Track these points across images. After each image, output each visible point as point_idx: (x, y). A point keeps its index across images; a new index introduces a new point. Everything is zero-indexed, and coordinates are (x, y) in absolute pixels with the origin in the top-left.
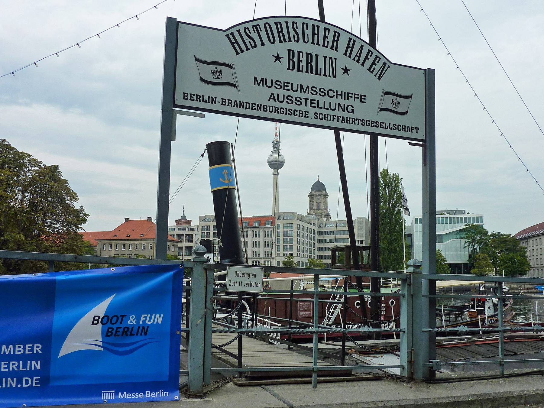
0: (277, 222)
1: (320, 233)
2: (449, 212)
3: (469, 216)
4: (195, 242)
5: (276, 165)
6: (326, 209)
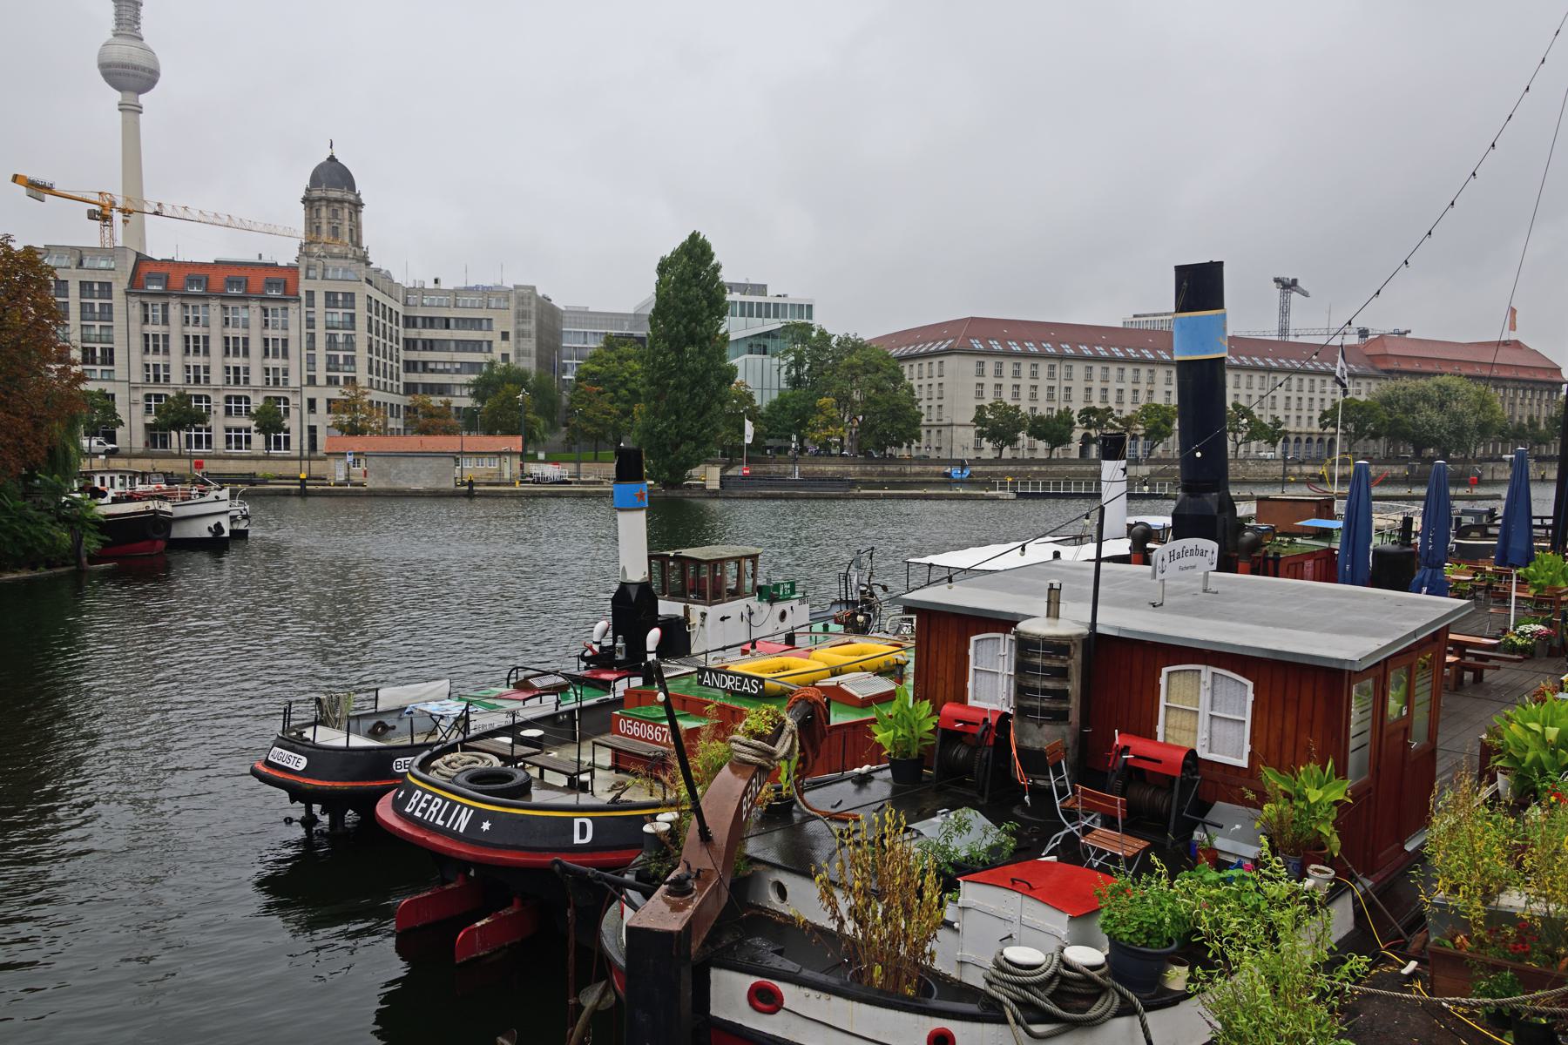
1: (410, 322)
5: (131, 78)
6: (358, 244)
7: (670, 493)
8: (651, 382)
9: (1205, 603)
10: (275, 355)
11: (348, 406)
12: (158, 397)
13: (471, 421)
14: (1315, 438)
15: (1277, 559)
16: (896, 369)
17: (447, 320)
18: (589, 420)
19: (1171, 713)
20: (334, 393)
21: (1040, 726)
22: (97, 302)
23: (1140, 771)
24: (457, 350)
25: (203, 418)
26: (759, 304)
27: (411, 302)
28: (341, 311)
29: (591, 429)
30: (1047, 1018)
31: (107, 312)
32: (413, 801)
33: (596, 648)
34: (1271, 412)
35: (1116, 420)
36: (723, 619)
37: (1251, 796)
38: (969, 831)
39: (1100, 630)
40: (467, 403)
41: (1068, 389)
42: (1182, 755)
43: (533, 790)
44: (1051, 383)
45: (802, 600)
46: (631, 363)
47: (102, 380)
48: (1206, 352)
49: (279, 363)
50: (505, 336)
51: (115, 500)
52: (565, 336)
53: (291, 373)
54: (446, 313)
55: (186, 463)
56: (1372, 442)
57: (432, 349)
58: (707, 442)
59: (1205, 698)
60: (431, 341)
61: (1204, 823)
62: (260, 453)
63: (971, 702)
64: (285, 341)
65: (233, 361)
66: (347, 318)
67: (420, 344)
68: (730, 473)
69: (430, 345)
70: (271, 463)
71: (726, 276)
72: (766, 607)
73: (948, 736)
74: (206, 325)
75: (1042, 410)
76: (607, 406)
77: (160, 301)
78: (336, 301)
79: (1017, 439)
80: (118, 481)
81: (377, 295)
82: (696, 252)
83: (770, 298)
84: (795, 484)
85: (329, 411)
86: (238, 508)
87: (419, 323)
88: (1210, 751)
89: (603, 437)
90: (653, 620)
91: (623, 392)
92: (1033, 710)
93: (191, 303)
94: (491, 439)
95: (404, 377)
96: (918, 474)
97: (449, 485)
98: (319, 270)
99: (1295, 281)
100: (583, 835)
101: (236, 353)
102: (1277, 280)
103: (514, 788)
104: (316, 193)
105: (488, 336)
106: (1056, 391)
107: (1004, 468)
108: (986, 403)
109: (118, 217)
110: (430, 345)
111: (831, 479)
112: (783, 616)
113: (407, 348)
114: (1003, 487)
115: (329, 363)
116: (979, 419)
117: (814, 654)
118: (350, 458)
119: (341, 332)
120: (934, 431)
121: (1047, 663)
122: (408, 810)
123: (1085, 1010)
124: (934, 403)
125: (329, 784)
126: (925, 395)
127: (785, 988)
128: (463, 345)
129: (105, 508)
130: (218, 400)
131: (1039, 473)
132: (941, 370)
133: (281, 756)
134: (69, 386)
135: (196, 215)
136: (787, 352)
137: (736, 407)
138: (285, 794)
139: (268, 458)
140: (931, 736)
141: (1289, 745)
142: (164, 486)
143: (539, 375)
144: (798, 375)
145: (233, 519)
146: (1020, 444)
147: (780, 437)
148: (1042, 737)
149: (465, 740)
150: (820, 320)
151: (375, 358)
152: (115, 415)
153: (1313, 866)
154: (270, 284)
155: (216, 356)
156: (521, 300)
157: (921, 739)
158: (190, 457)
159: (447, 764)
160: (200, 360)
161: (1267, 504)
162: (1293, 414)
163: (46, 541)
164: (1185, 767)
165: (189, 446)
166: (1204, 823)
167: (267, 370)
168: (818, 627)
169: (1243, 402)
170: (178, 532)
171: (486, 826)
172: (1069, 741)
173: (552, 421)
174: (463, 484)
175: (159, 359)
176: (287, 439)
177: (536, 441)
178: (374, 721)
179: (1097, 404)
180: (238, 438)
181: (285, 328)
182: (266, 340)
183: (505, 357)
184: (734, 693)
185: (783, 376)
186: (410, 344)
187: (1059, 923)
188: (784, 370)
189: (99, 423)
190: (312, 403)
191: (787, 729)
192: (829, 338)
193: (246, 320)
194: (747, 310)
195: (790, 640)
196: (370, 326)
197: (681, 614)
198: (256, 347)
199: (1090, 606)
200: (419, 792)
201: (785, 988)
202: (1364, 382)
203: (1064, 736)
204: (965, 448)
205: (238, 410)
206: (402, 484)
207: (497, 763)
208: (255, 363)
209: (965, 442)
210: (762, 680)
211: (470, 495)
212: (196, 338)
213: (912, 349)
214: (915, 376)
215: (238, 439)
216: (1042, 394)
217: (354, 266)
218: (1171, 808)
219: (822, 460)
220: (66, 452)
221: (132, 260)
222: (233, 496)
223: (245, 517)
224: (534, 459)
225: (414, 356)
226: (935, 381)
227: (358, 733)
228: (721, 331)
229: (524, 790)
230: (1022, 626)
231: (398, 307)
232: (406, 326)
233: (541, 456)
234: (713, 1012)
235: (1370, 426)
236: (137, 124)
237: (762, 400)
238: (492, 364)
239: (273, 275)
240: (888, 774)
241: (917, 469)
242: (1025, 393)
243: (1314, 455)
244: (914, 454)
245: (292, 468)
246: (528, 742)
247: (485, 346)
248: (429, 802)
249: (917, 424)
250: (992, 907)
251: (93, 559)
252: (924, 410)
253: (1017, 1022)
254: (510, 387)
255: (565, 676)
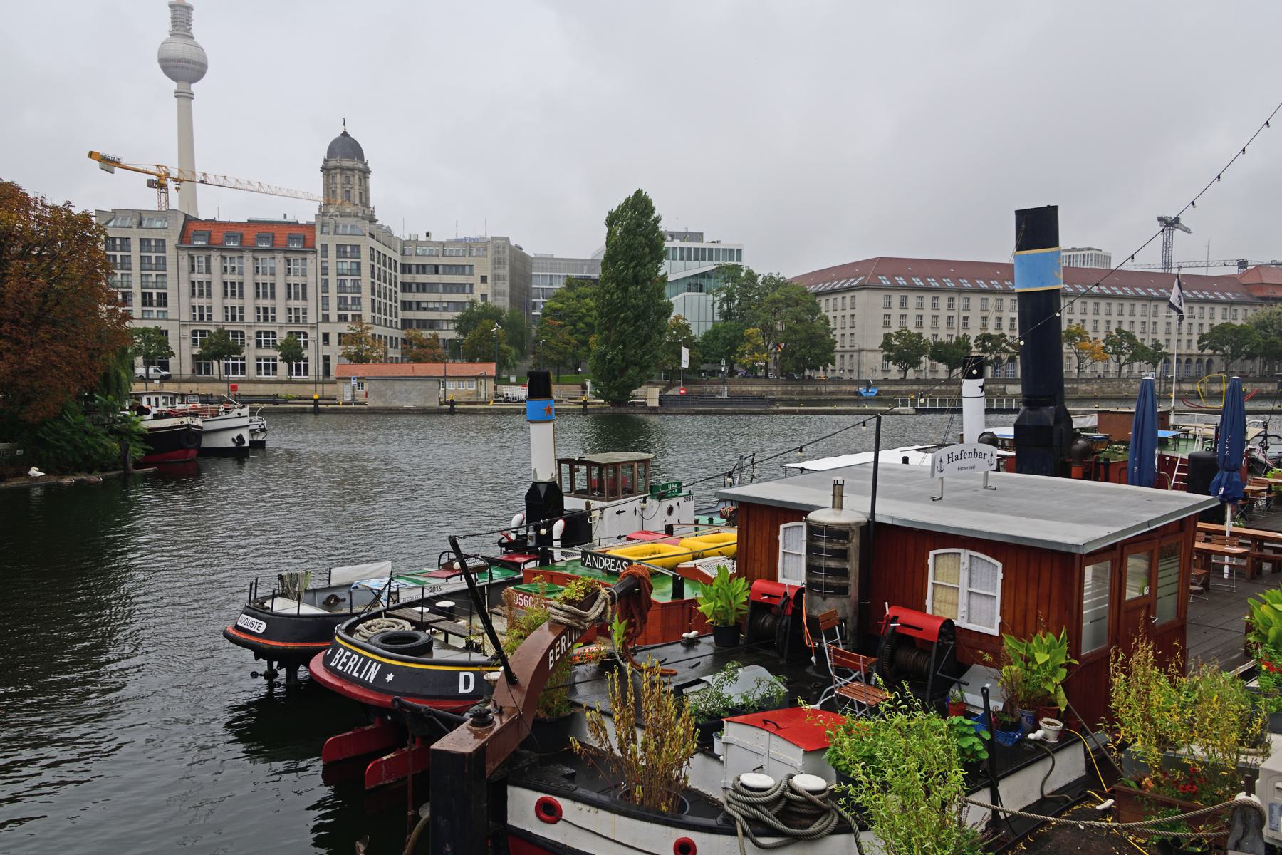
1: (406, 269)
5: (184, 70)
6: (366, 205)
7: (617, 410)
8: (601, 315)
9: (987, 497)
10: (296, 298)
11: (355, 339)
12: (203, 333)
13: (455, 351)
14: (1194, 359)
15: (1107, 464)
16: (814, 303)
17: (437, 267)
18: (552, 349)
19: (938, 589)
20: (344, 328)
21: (825, 599)
22: (153, 255)
23: (911, 638)
24: (445, 292)
25: (237, 350)
26: (696, 250)
27: (407, 252)
28: (349, 260)
29: (554, 357)
30: (773, 832)
31: (162, 263)
32: (337, 657)
33: (513, 536)
34: (1152, 336)
35: (1009, 344)
36: (619, 513)
37: (988, 657)
38: (750, 682)
39: (878, 519)
40: (453, 335)
41: (966, 318)
42: (940, 623)
43: (434, 649)
44: (951, 313)
45: (688, 497)
46: (588, 300)
47: (158, 319)
48: (1043, 284)
49: (299, 304)
50: (484, 279)
51: (156, 417)
54: (435, 261)
55: (225, 386)
56: (1249, 362)
57: (424, 291)
58: (648, 367)
59: (964, 577)
60: (424, 284)
61: (960, 683)
62: (284, 379)
63: (781, 580)
64: (304, 286)
65: (263, 303)
66: (355, 266)
67: (414, 287)
68: (670, 392)
69: (423, 288)
70: (293, 386)
71: (663, 227)
72: (655, 503)
73: (757, 607)
74: (241, 274)
75: (943, 337)
76: (567, 337)
77: (204, 254)
78: (345, 252)
79: (919, 363)
80: (161, 401)
81: (378, 247)
82: (639, 207)
83: (706, 244)
84: (723, 402)
85: (340, 343)
86: (257, 422)
87: (413, 269)
88: (969, 621)
89: (563, 363)
90: (558, 511)
91: (581, 325)
92: (818, 585)
93: (228, 255)
94: (470, 365)
95: (401, 315)
96: (832, 393)
97: (434, 404)
98: (332, 227)
99: (1177, 219)
100: (467, 686)
101: (265, 296)
102: (1160, 219)
103: (417, 647)
104: (332, 163)
105: (470, 280)
106: (955, 320)
107: (909, 388)
108: (892, 331)
109: (171, 185)
110: (423, 288)
111: (754, 398)
112: (670, 510)
113: (404, 290)
114: (904, 404)
115: (339, 303)
116: (886, 345)
117: (683, 541)
118: (354, 382)
119: (349, 278)
120: (847, 356)
121: (830, 546)
122: (333, 664)
123: (807, 827)
124: (848, 332)
125: (282, 644)
126: (839, 326)
127: (564, 803)
128: (449, 288)
129: (148, 423)
130: (250, 335)
131: (940, 392)
132: (853, 303)
133: (248, 622)
134: (118, 324)
135: (233, 183)
136: (720, 289)
137: (676, 337)
138: (249, 654)
139: (290, 382)
140: (745, 607)
141: (1031, 616)
142: (199, 405)
143: (511, 311)
144: (729, 309)
145: (253, 432)
146: (923, 366)
147: (713, 362)
148: (826, 607)
149: (388, 609)
150: (747, 262)
151: (377, 299)
152: (168, 348)
153: (1045, 720)
154: (292, 238)
155: (246, 298)
156: (497, 249)
157: (738, 610)
158: (228, 382)
159: (368, 628)
160: (236, 302)
161: (1107, 416)
162: (1174, 337)
163: (100, 450)
164: (941, 633)
165: (227, 372)
166: (960, 683)
167: (290, 309)
168: (704, 520)
169: (1126, 328)
170: (207, 443)
171: (390, 677)
172: (849, 611)
173: (522, 351)
174: (446, 403)
175: (203, 301)
176: (306, 367)
177: (508, 367)
178: (328, 594)
179: (992, 331)
180: (266, 366)
181: (304, 275)
182: (289, 285)
183: (484, 297)
184: (609, 573)
185: (716, 310)
186: (406, 287)
187: (794, 755)
188: (717, 305)
189: (155, 354)
190: (326, 337)
191: (601, 597)
192: (756, 277)
193: (272, 269)
194: (686, 255)
195: (669, 530)
196: (373, 272)
197: (584, 508)
198: (281, 291)
199: (870, 499)
200: (342, 650)
201: (564, 803)
202: (1240, 309)
203: (844, 606)
204: (874, 370)
205: (267, 343)
206: (397, 403)
207: (408, 627)
208: (249, 303)
209: (873, 365)
210: (630, 562)
211: (452, 412)
212: (233, 284)
213: (828, 286)
214: (831, 308)
215: (267, 367)
216: (943, 323)
217: (360, 223)
218: (933, 667)
219: (749, 381)
220: (118, 378)
221: (181, 220)
222: (252, 413)
223: (263, 430)
224: (507, 382)
225: (409, 297)
226: (848, 313)
227: (306, 603)
228: (661, 273)
229: (426, 649)
230: (811, 516)
231: (397, 257)
232: (403, 272)
233: (513, 379)
234: (510, 822)
235: (1246, 348)
237: (697, 331)
238: (473, 303)
239: (294, 231)
240: (712, 639)
241: (832, 388)
242: (927, 322)
243: (1192, 373)
244: (829, 375)
245: (308, 390)
246: (441, 611)
247: (467, 288)
248: (348, 658)
249: (832, 349)
250: (748, 743)
251: (138, 465)
252: (838, 338)
253: (745, 834)
254: (487, 322)
255: (484, 558)
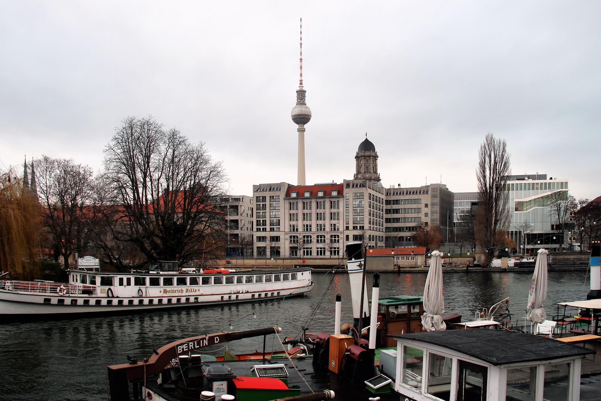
0: (346, 191)
2: (529, 177)
3: (551, 181)
4: (241, 215)
5: (302, 119)
6: (376, 172)
52: (455, 204)
53: (312, 226)
67: (392, 211)
70: (331, 261)
81: (373, 192)
83: (548, 181)
104: (360, 154)
113: (387, 213)
190: (347, 237)
215: (335, 252)
236: (303, 135)
